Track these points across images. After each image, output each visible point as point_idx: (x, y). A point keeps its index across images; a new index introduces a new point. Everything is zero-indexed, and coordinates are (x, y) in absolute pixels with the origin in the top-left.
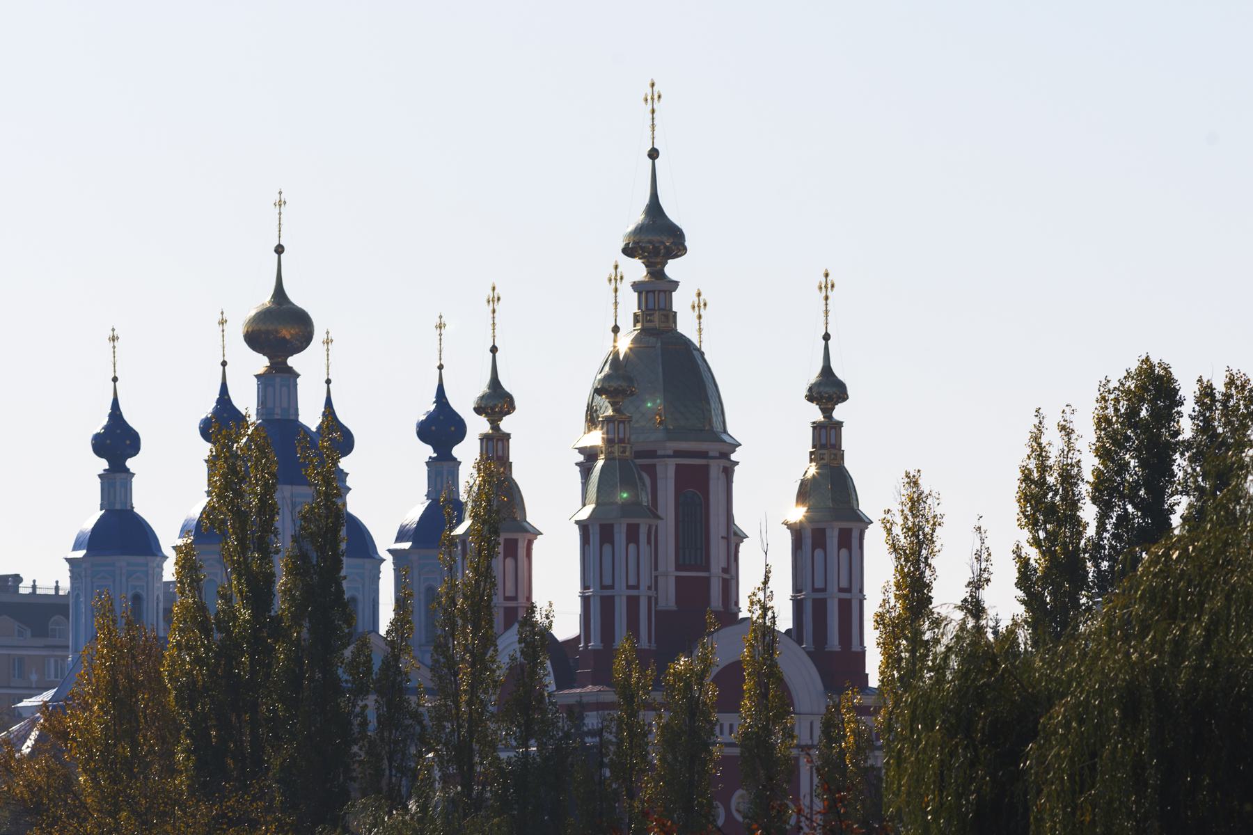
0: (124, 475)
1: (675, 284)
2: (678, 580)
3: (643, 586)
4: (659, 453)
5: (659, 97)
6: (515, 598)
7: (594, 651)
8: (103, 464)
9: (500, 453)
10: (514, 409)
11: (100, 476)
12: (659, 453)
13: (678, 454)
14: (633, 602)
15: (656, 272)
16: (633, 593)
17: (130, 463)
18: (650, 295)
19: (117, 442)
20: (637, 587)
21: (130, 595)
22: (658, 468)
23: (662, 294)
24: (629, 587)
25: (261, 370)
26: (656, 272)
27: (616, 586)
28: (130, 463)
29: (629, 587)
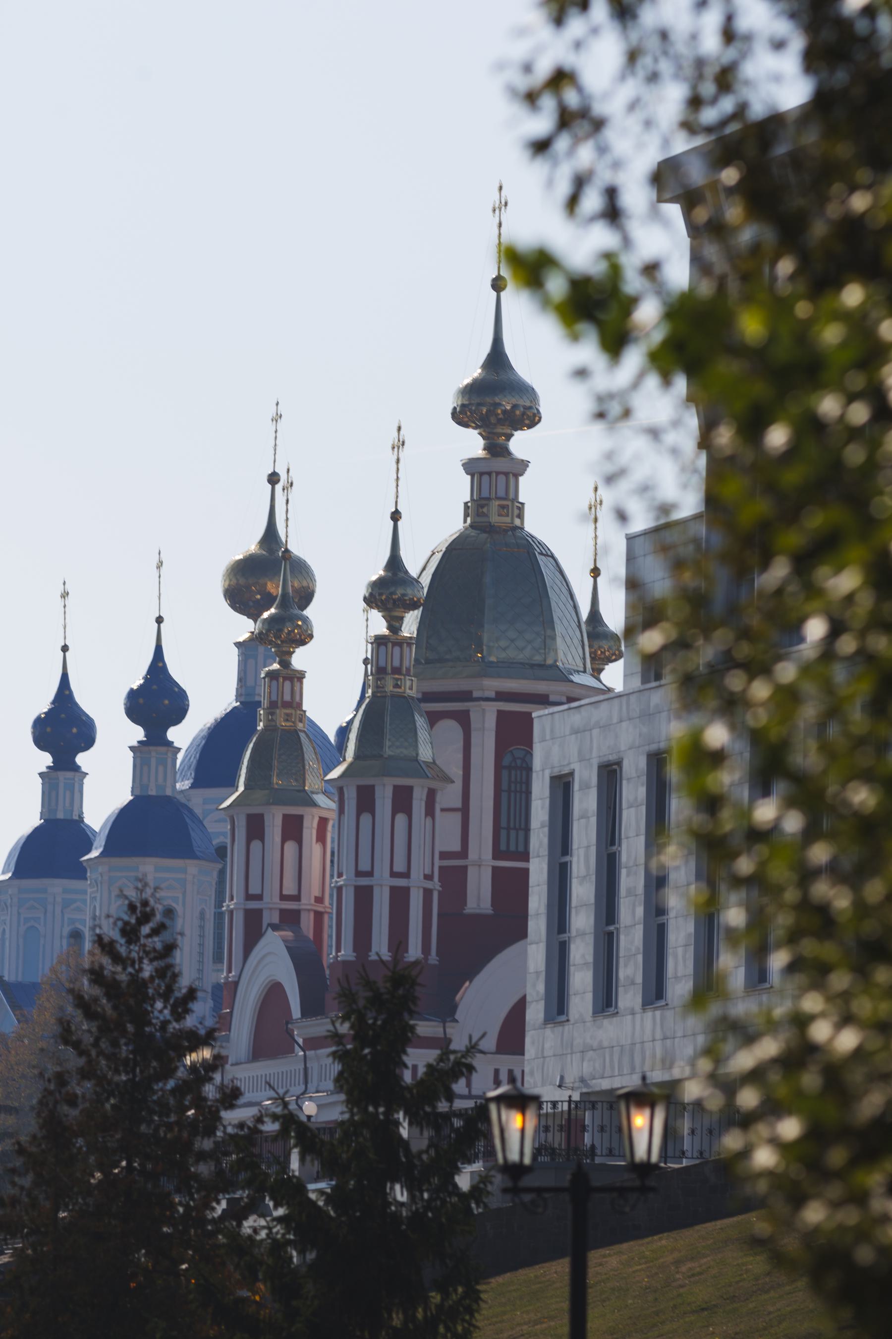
0: (69, 774)
1: (524, 465)
2: (495, 869)
3: (417, 874)
4: (476, 694)
5: (494, 211)
6: (297, 898)
7: (345, 963)
8: (46, 759)
9: (287, 698)
10: (311, 637)
11: (41, 775)
12: (476, 694)
13: (501, 696)
14: (400, 898)
15: (497, 448)
16: (401, 882)
17: (82, 759)
18: (485, 478)
19: (63, 730)
20: (406, 875)
21: (66, 931)
22: (473, 716)
23: (502, 478)
24: (393, 874)
25: (244, 636)
26: (497, 448)
27: (376, 873)
28: (82, 759)
29: (393, 874)
